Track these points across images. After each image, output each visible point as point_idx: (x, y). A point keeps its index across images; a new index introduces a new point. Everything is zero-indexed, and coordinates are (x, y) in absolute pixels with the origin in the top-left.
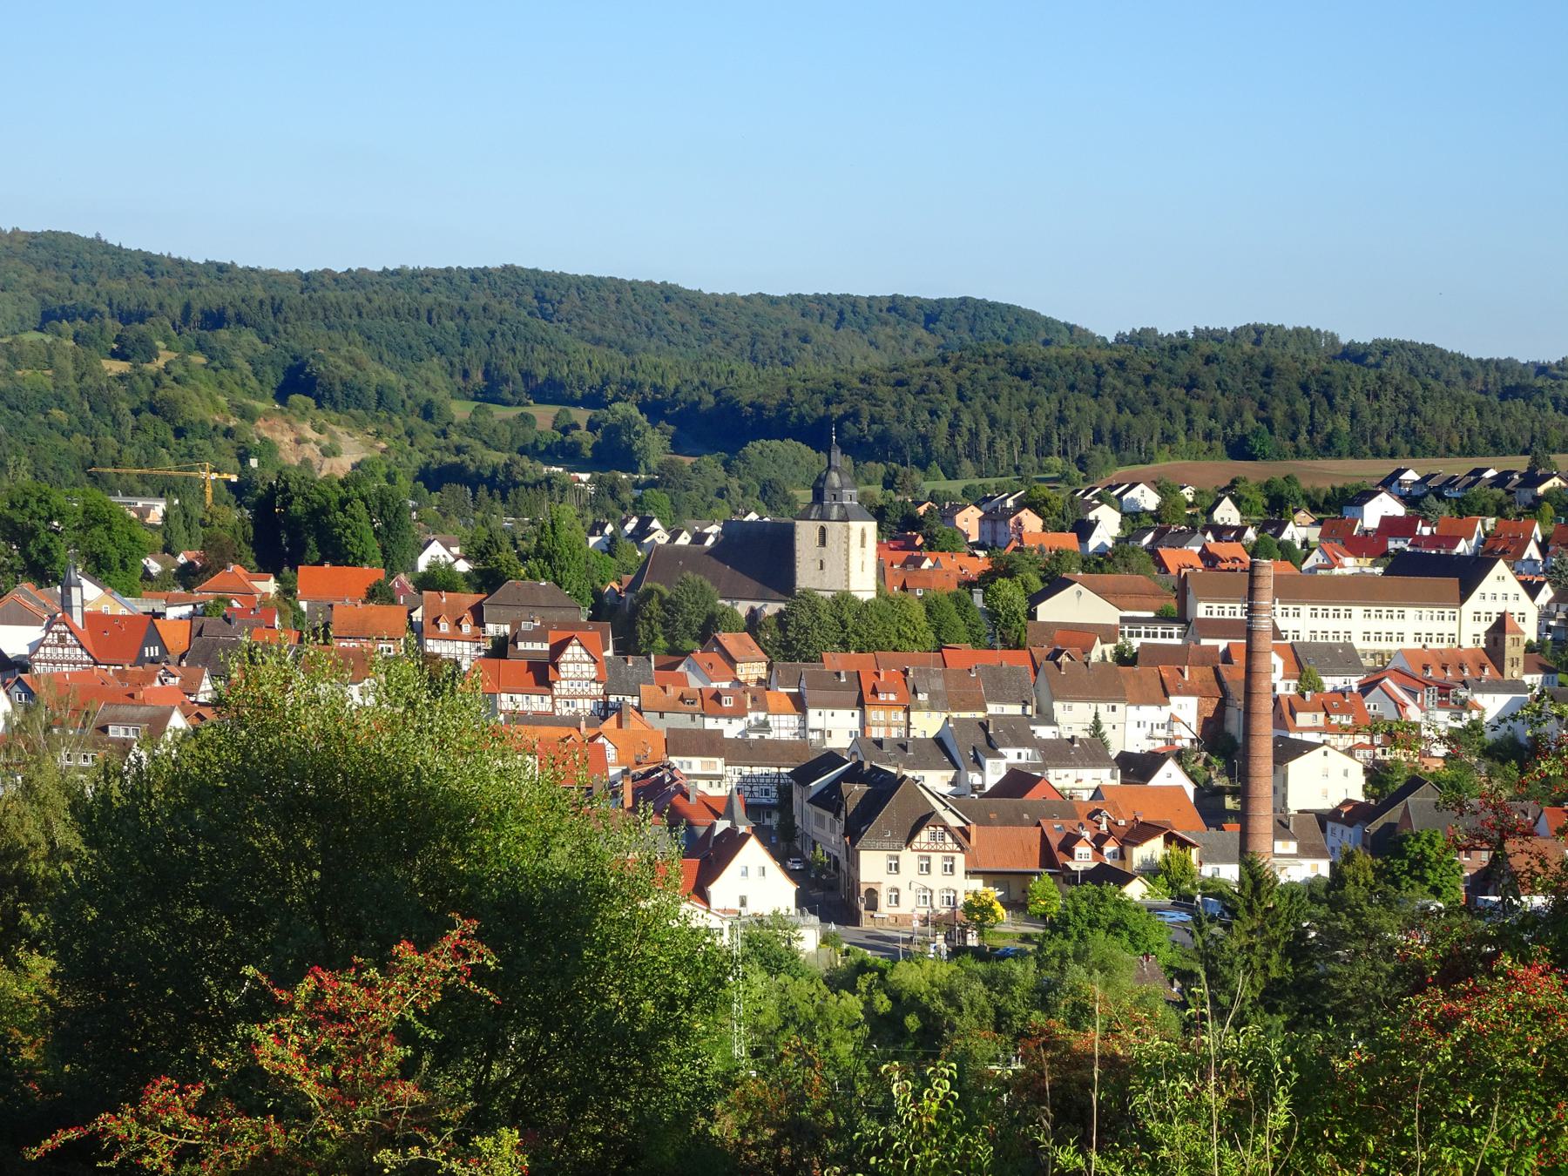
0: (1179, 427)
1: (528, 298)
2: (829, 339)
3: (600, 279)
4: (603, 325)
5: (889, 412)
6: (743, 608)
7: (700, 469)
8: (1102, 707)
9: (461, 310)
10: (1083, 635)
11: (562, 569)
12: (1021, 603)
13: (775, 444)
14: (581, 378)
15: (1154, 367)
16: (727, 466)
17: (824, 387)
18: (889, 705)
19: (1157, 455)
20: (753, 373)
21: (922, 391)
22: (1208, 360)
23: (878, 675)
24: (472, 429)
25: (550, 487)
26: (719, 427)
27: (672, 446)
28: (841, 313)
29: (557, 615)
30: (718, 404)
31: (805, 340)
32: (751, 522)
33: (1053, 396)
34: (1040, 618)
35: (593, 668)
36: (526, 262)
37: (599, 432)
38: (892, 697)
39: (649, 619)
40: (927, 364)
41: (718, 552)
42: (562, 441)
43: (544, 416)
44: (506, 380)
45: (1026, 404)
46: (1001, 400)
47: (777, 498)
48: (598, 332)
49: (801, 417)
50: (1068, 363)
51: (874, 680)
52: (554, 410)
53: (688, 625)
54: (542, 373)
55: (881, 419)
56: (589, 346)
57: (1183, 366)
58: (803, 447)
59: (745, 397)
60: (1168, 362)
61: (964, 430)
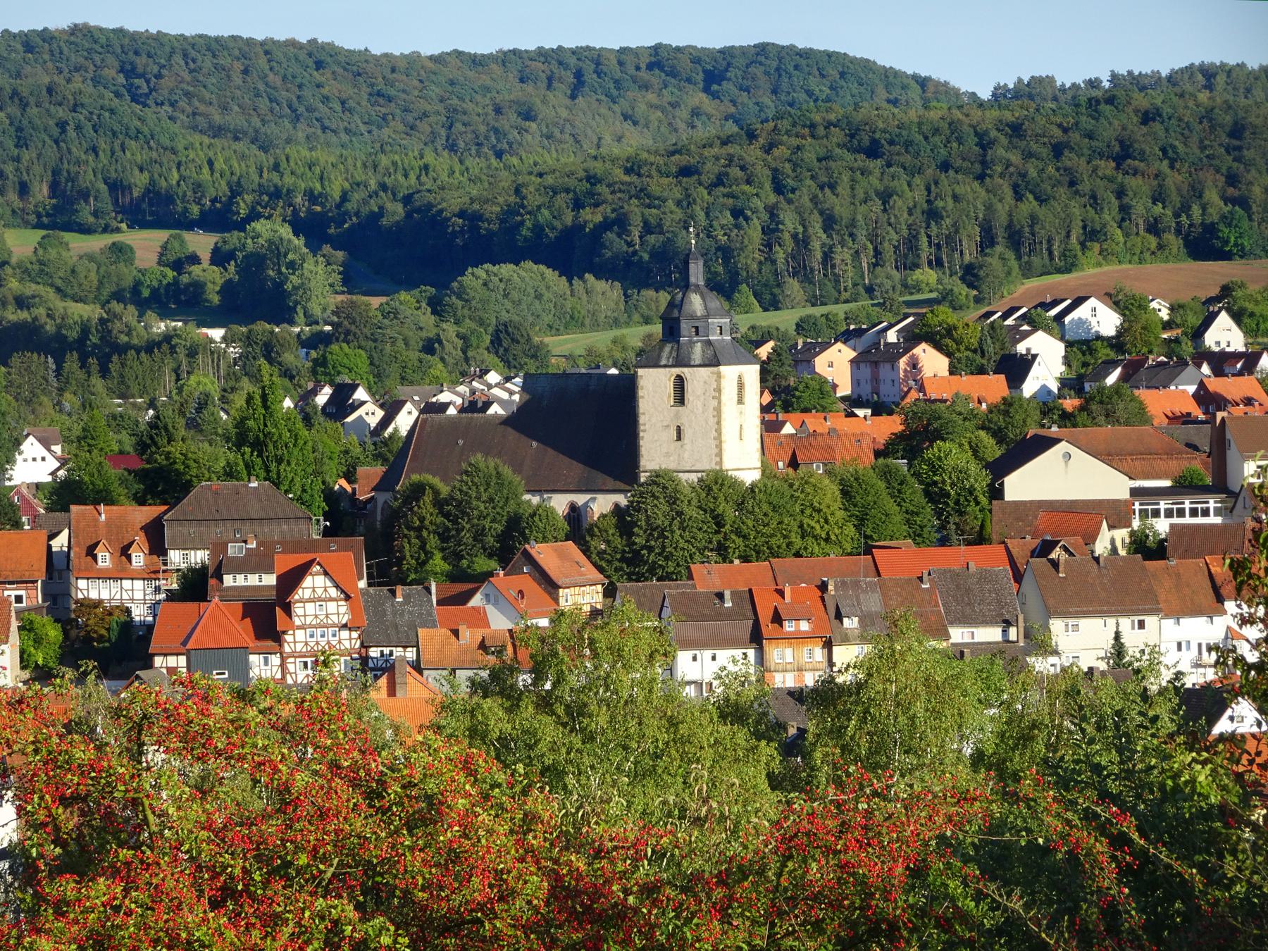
0: (1109, 217)
1: (110, 73)
2: (564, 113)
3: (217, 40)
4: (225, 108)
5: (672, 214)
6: (559, 503)
7: (396, 313)
8: (1125, 623)
9: (15, 93)
10: (1084, 516)
11: (279, 461)
12: (979, 479)
13: (506, 269)
14: (198, 187)
15: (1065, 130)
16: (437, 307)
17: (571, 183)
18: (800, 638)
19: (1082, 260)
20: (457, 167)
21: (719, 181)
22: (1147, 118)
23: (781, 593)
24: (39, 270)
25: (173, 349)
26: (414, 250)
27: (345, 282)
28: (579, 75)
29: (276, 531)
30: (409, 215)
31: (528, 116)
32: (613, 375)
33: (917, 180)
34: (1010, 495)
35: (343, 609)
36: (106, 19)
37: (232, 267)
38: (804, 626)
39: (419, 529)
40: (725, 143)
41: (519, 420)
42: (176, 282)
43: (146, 245)
44: (85, 195)
45: (878, 194)
46: (839, 189)
47: (517, 350)
48: (218, 118)
49: (538, 229)
50: (936, 131)
51: (776, 601)
52: (160, 236)
53: (479, 535)
54: (139, 181)
55: (660, 225)
56: (206, 140)
57: (1110, 127)
58: (549, 272)
59: (452, 202)
60: (1086, 122)
61: (787, 236)
